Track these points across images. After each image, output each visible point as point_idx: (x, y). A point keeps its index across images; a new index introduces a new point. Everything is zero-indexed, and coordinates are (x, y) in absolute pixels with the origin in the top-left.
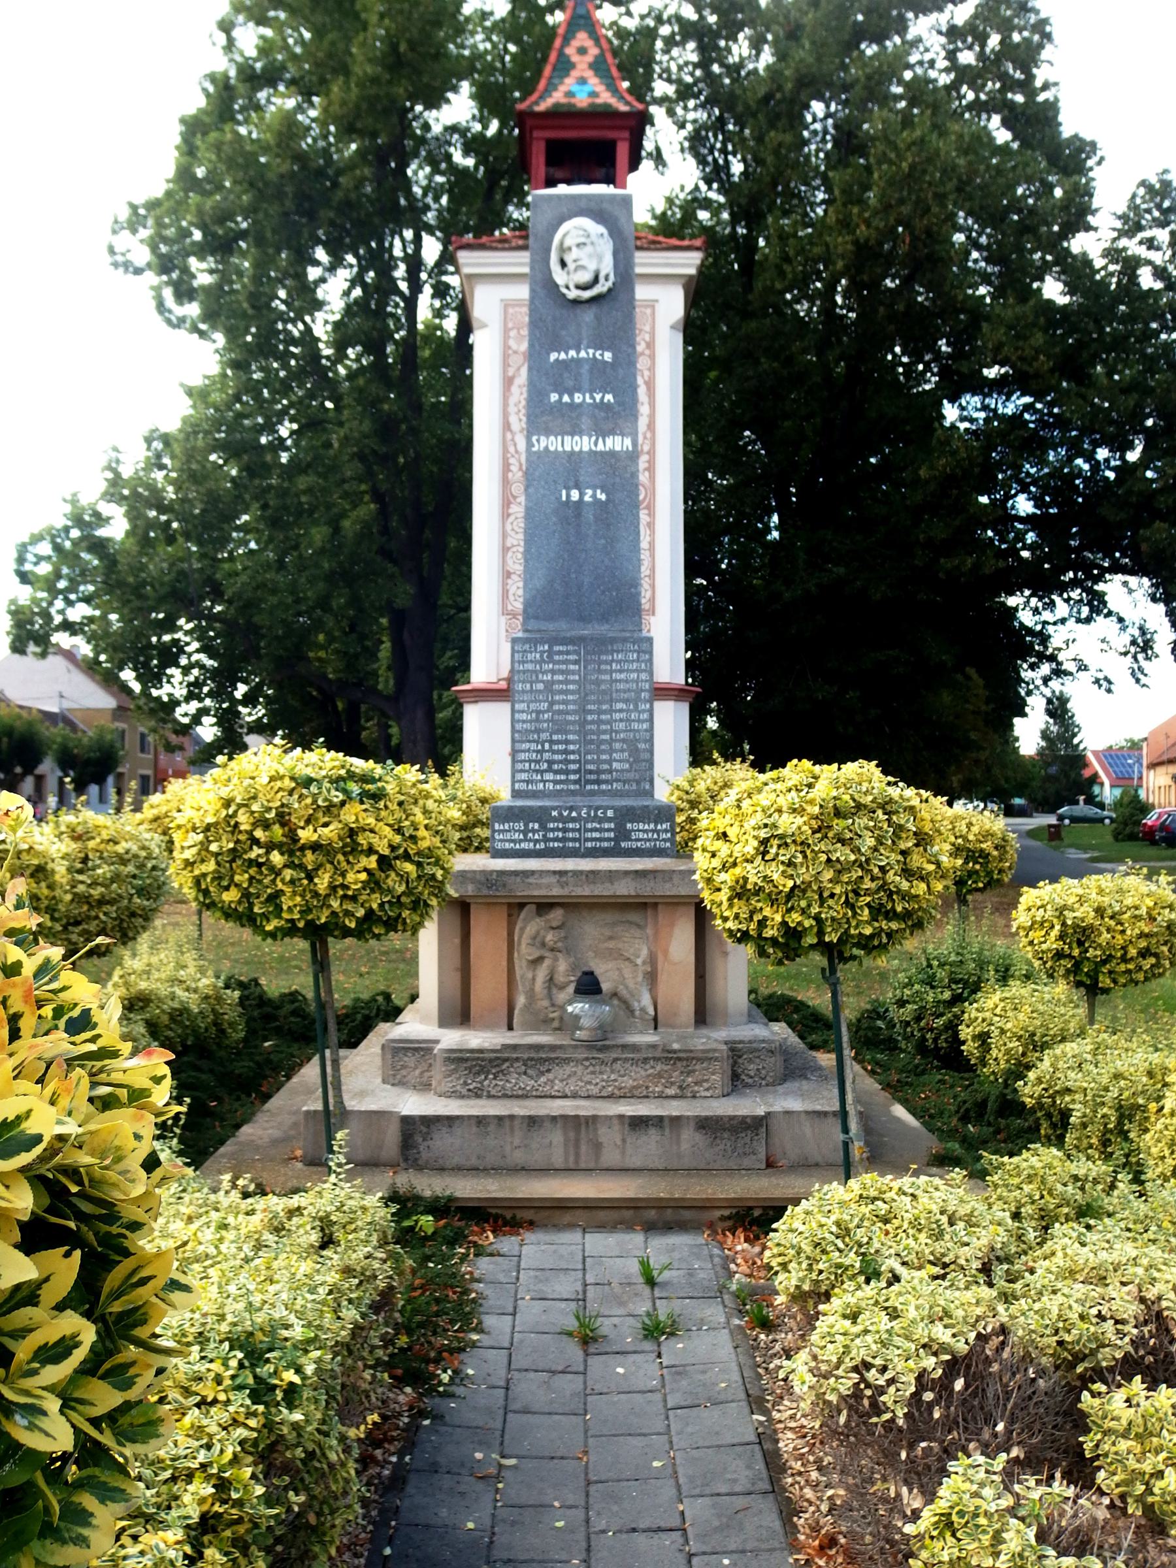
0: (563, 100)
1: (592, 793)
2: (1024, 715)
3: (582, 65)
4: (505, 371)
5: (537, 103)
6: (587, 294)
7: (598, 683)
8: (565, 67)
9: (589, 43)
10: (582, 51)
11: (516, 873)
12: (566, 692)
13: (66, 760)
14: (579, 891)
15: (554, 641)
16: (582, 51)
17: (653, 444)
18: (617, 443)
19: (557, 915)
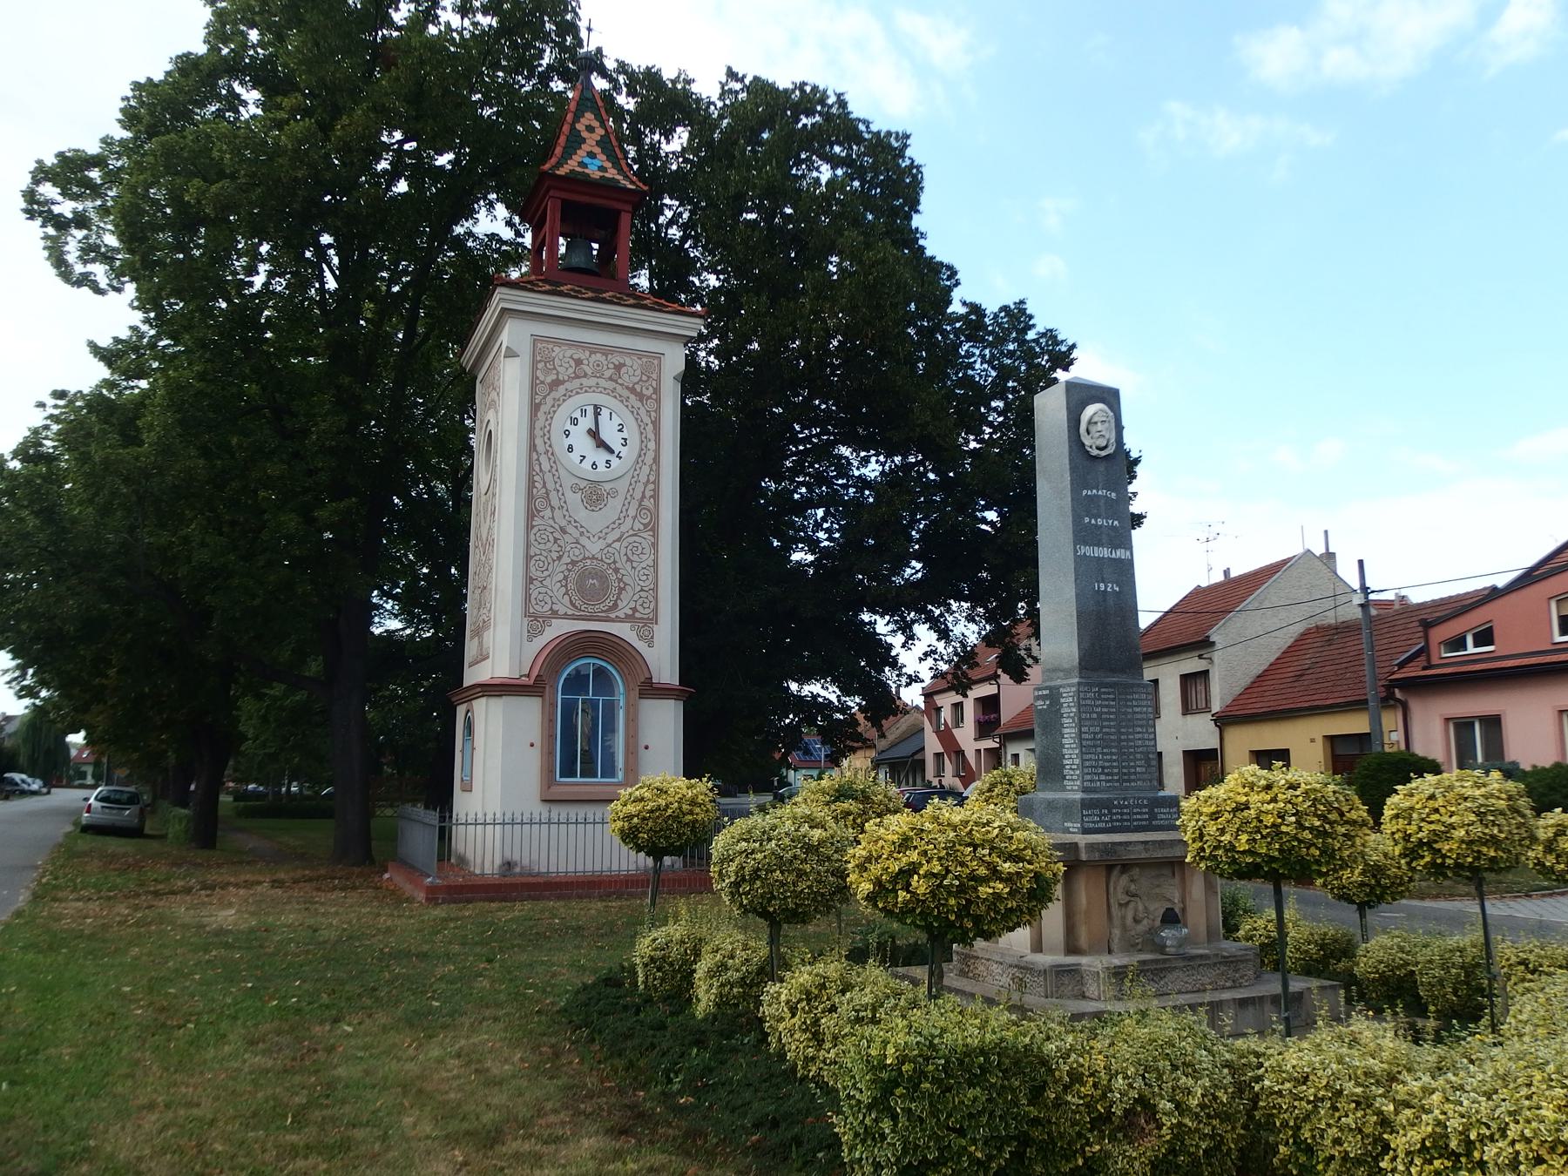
1: (1127, 789)
3: (591, 141)
5: (559, 165)
6: (1103, 453)
7: (1126, 713)
8: (576, 141)
9: (596, 124)
11: (1120, 844)
12: (1109, 720)
14: (1155, 855)
15: (1101, 685)
16: (590, 129)
17: (658, 475)
18: (1120, 554)
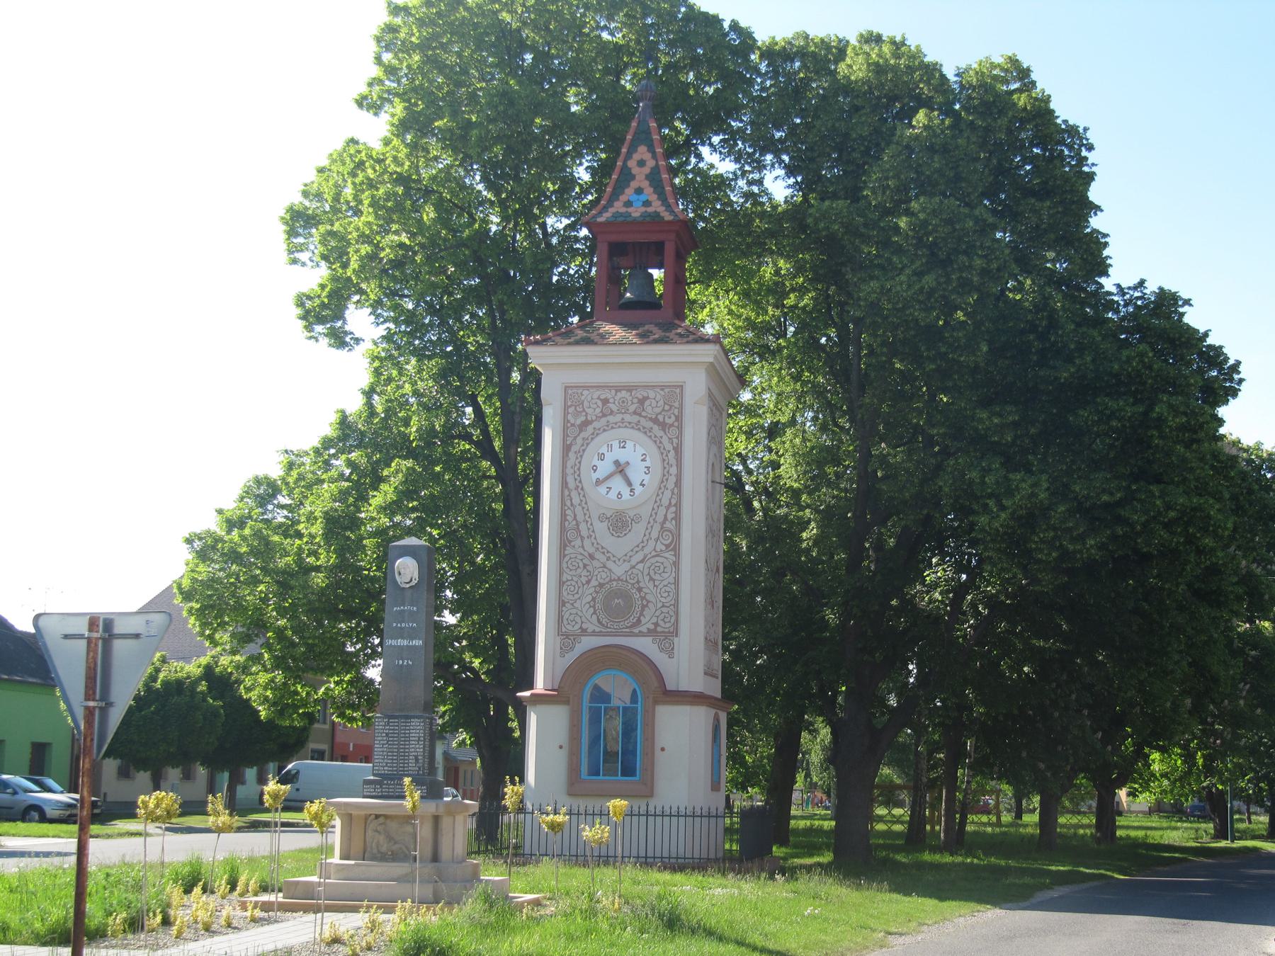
0: (623, 210)
2: (1098, 208)
4: (564, 440)
9: (647, 156)
10: (641, 163)
13: (705, 930)
16: (641, 163)
19: (381, 820)
